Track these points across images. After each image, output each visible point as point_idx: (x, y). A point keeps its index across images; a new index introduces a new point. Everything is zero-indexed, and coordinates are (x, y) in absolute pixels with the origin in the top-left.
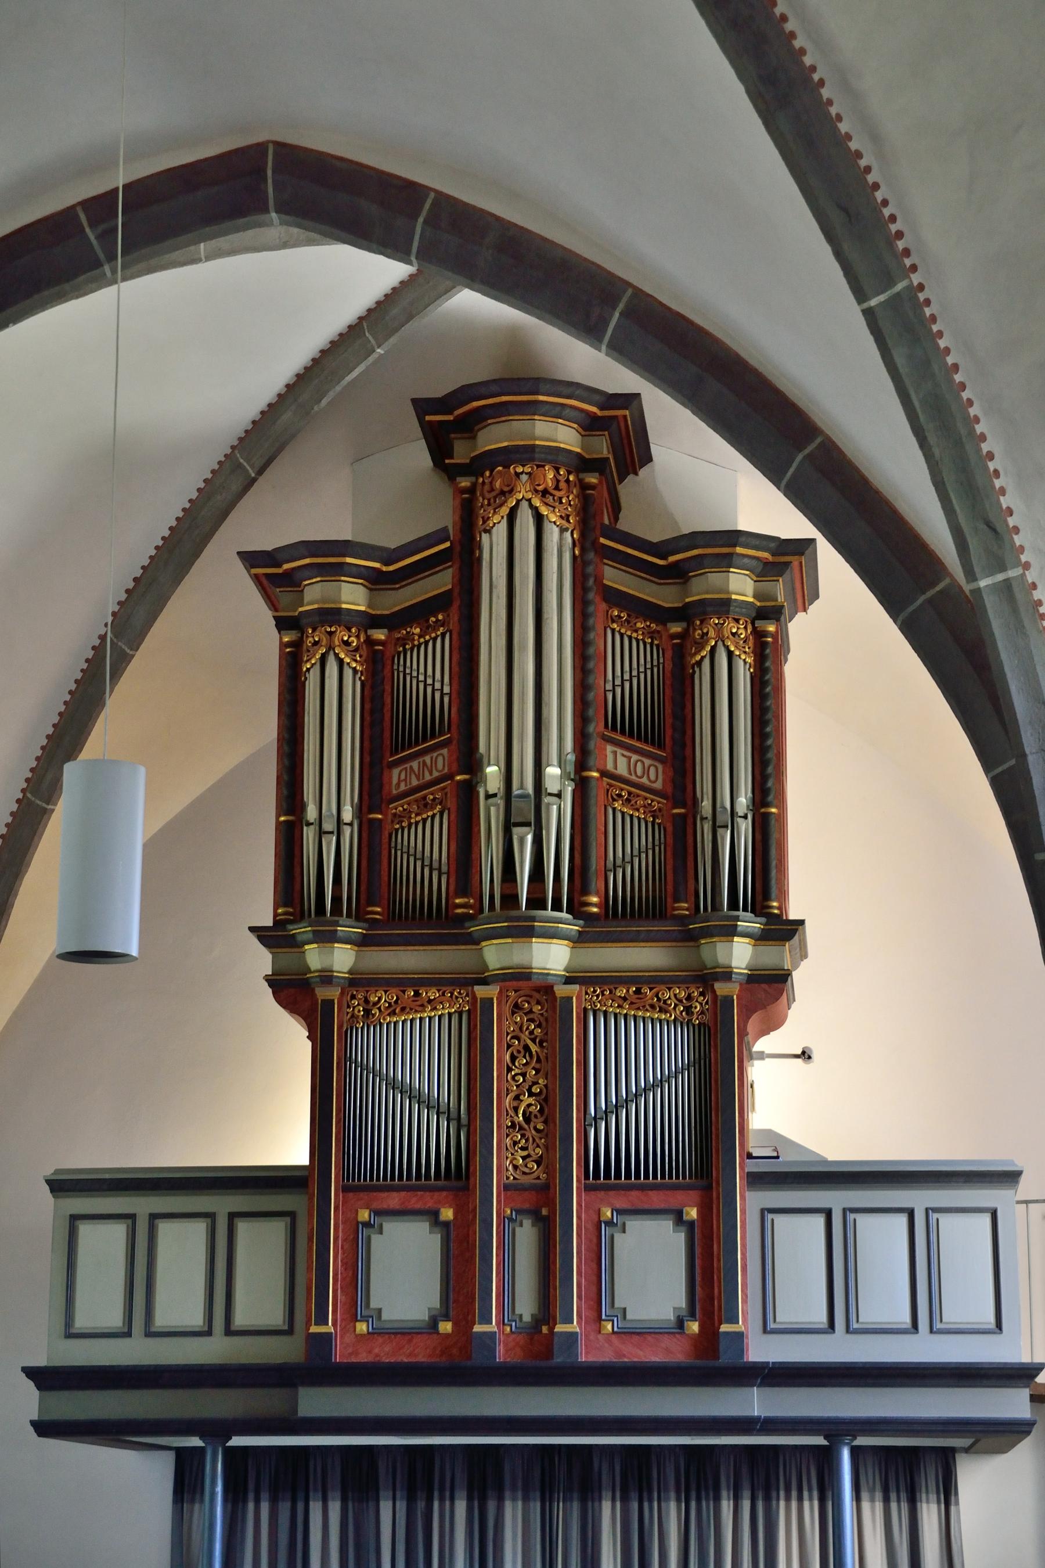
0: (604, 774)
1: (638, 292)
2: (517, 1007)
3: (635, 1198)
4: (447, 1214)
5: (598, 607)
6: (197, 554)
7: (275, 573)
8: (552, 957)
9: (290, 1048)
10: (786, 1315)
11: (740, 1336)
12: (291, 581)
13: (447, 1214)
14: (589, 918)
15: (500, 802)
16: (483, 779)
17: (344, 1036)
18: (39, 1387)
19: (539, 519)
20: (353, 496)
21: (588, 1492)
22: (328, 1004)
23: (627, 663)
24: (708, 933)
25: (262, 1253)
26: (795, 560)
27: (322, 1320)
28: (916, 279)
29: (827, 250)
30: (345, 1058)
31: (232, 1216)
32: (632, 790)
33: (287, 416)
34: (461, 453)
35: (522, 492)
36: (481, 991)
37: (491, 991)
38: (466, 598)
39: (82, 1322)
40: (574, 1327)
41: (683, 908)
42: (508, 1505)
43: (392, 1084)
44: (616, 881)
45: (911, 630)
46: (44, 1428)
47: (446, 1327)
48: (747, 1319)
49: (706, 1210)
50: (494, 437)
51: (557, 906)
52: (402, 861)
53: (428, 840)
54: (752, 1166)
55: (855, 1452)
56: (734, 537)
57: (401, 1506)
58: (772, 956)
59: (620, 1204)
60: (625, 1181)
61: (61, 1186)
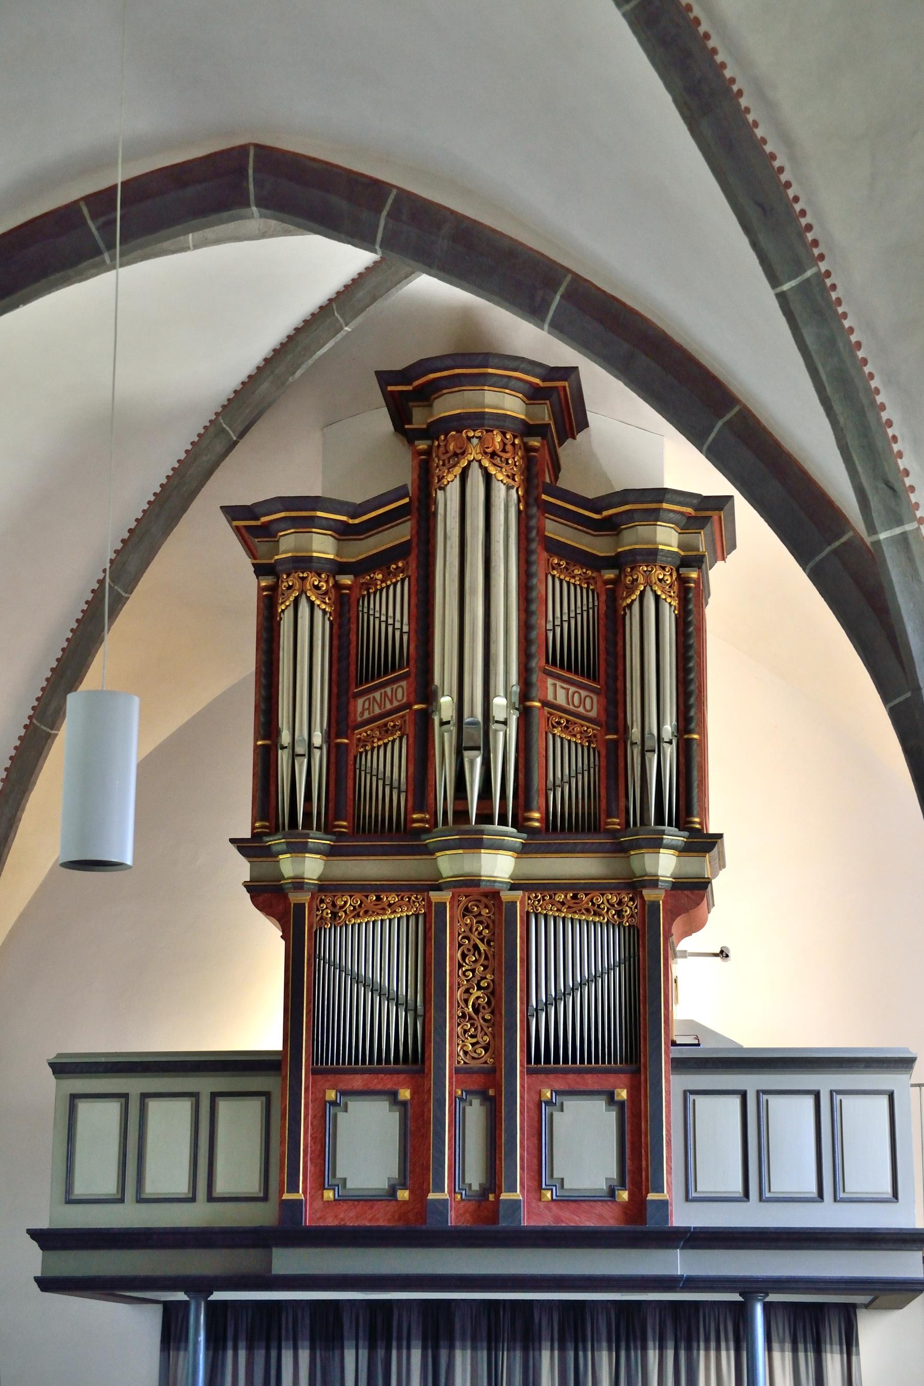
0: (545, 703)
1: (577, 277)
2: (467, 910)
4: (405, 1094)
5: (541, 557)
6: (184, 509)
7: (254, 525)
8: (498, 866)
10: (705, 1186)
12: (268, 532)
13: (405, 1094)
15: (453, 728)
17: (314, 936)
18: (42, 1247)
21: (529, 1342)
22: (300, 907)
23: (566, 606)
24: (637, 845)
25: (240, 1127)
26: (715, 515)
27: (294, 1188)
28: (823, 266)
30: (314, 955)
31: (214, 1096)
34: (419, 419)
35: (474, 453)
36: (435, 896)
37: (445, 896)
39: (80, 1189)
40: (518, 1195)
41: (615, 823)
42: (458, 1353)
44: (556, 799)
45: (818, 577)
46: (46, 1284)
48: (671, 1190)
50: (448, 405)
51: (503, 821)
52: (366, 781)
53: (389, 762)
54: (675, 1053)
56: (661, 494)
57: (364, 1354)
58: (693, 866)
59: (560, 1085)
61: (62, 1068)
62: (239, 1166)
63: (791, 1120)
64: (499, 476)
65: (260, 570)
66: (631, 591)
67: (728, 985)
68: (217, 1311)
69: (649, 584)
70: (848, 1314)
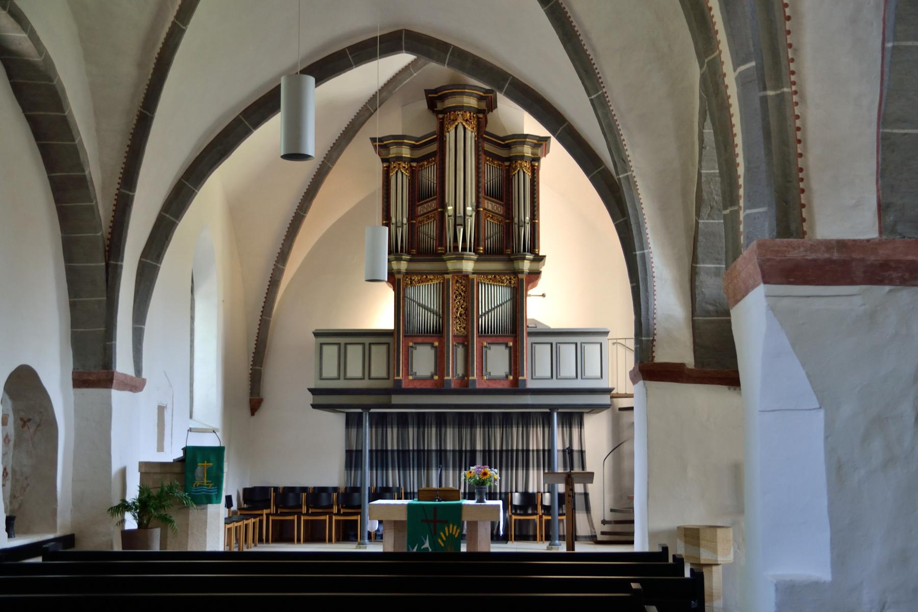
0: (484, 209)
1: (514, 78)
2: (457, 281)
3: (494, 340)
4: (436, 344)
5: (483, 156)
6: (353, 136)
7: (382, 145)
8: (468, 266)
9: (387, 295)
10: (538, 374)
11: (525, 381)
12: (386, 147)
13: (436, 344)
14: (480, 254)
15: (453, 218)
16: (447, 210)
17: (404, 290)
18: (313, 394)
19: (465, 129)
20: (402, 120)
21: (472, 425)
22: (399, 280)
23: (491, 175)
24: (517, 259)
25: (379, 354)
26: (544, 143)
27: (398, 375)
28: (604, 90)
29: (580, 82)
30: (404, 297)
31: (370, 344)
32: (494, 215)
33: (384, 94)
34: (440, 106)
35: (460, 120)
36: (446, 276)
37: (450, 276)
38: (441, 154)
39: (325, 375)
40: (475, 377)
41: (509, 251)
42: (448, 430)
43: (419, 305)
44: (488, 243)
45: (592, 180)
46: (314, 406)
47: (436, 378)
48: (526, 375)
49: (515, 342)
50: (450, 103)
51: (470, 251)
52: (421, 235)
53: (429, 229)
54: (529, 330)
55: (558, 413)
56: (526, 136)
57: (416, 430)
58: (535, 266)
59: (489, 341)
60: (490, 335)
61: (317, 334)
62: (379, 369)
63: (568, 353)
64: (469, 128)
65: (384, 160)
66: (515, 169)
67: (545, 306)
68: (371, 415)
69: (521, 167)
70: (581, 417)
